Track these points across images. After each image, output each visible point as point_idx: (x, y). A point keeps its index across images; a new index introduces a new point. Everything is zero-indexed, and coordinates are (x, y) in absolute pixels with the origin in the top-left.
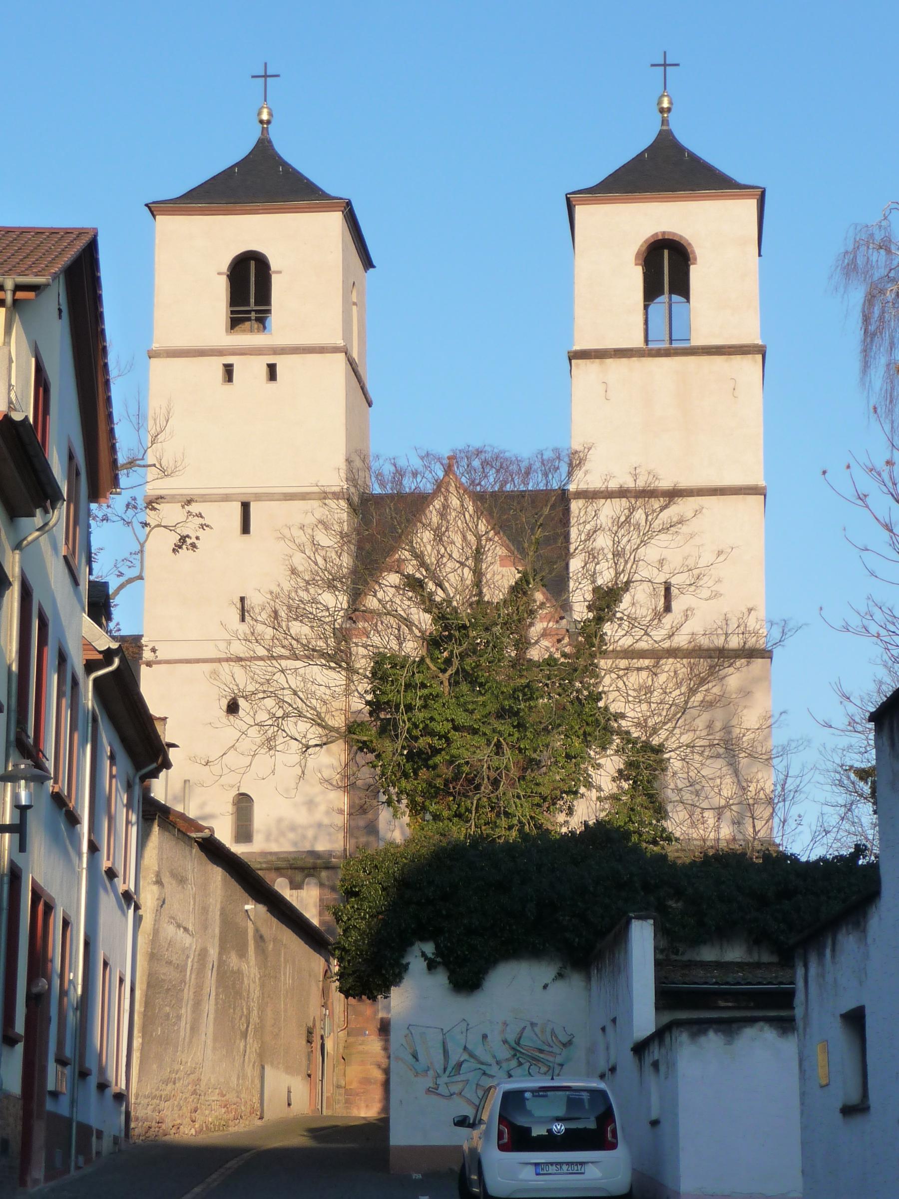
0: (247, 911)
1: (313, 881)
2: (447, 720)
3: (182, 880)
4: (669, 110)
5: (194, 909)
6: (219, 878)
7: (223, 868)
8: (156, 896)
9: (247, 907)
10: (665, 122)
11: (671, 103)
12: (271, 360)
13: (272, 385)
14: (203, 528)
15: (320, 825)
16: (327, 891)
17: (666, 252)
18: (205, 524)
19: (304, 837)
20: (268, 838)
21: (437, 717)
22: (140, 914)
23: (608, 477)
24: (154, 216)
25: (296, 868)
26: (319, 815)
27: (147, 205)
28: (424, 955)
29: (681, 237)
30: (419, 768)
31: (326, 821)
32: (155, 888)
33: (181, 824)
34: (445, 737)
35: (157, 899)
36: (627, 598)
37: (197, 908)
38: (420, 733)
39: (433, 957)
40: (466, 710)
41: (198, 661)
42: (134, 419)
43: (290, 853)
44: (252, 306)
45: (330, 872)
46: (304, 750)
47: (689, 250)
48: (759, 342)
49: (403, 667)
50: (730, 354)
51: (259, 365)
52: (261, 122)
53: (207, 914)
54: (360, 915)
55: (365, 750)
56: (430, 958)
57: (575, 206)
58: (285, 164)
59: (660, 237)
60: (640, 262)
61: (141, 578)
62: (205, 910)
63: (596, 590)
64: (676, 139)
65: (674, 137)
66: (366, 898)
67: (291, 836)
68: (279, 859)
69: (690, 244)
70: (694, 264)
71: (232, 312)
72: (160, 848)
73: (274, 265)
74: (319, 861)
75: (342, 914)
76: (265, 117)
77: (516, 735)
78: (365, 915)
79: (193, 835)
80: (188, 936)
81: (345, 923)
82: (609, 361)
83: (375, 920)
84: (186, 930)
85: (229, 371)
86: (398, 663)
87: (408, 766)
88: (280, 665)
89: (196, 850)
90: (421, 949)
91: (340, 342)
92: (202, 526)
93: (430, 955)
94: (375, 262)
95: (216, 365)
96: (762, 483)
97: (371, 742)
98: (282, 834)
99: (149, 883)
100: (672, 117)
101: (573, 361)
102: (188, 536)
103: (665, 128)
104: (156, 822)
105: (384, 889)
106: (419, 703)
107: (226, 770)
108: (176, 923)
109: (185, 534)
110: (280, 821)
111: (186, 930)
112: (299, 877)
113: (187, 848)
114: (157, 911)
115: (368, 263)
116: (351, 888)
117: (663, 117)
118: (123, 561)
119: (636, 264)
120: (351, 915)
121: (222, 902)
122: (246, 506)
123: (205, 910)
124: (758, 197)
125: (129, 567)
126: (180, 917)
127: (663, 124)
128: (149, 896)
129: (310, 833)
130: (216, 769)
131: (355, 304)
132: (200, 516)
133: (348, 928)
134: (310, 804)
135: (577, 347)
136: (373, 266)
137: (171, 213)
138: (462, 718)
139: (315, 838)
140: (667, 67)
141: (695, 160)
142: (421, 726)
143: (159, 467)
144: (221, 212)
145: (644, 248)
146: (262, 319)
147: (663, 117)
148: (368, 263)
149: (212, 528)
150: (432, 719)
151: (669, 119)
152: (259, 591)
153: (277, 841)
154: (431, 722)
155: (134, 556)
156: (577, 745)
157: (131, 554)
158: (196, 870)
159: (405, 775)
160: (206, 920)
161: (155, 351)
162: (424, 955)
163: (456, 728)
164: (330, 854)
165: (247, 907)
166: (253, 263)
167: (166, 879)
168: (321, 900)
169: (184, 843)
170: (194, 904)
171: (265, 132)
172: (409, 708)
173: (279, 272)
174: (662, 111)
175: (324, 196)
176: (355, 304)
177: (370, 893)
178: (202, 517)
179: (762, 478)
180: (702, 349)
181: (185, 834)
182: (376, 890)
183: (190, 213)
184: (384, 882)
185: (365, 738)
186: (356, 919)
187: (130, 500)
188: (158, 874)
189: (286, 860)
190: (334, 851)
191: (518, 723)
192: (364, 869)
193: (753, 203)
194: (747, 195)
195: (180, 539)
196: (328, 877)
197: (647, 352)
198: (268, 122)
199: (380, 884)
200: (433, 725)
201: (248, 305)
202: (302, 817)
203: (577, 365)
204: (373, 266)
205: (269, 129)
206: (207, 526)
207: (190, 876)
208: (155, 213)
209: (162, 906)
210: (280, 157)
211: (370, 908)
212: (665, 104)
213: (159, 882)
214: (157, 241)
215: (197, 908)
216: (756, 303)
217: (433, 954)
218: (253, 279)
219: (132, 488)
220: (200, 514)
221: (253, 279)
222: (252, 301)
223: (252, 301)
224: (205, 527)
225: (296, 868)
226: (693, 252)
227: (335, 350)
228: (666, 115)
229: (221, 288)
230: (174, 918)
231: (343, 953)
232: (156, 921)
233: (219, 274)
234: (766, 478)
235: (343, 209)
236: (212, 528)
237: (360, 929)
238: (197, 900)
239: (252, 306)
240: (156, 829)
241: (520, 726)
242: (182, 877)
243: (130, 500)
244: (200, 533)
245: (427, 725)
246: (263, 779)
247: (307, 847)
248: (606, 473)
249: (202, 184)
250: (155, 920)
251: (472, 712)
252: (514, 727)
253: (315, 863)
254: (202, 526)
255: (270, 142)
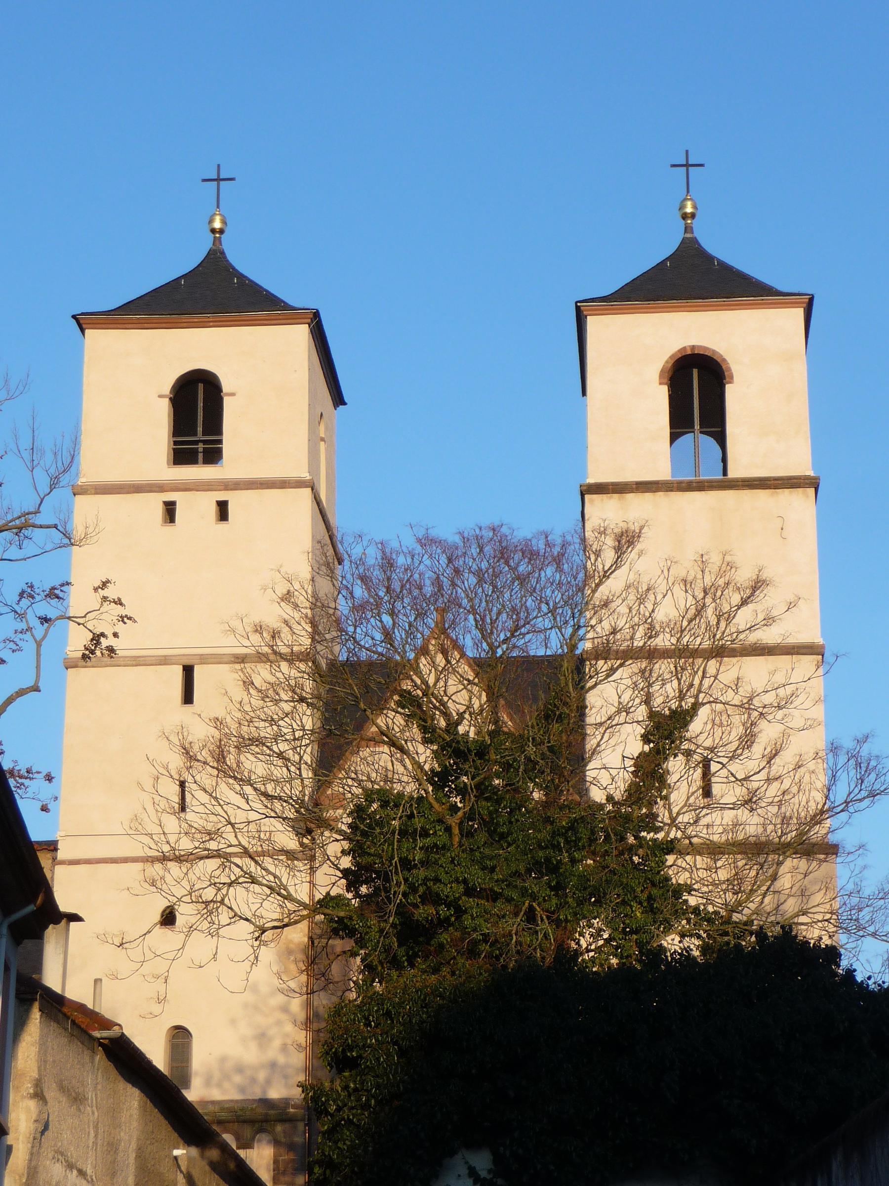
0: (176, 1158)
1: (264, 1137)
2: (457, 881)
3: (77, 1099)
4: (693, 216)
5: (95, 1143)
6: (136, 1104)
7: (142, 1090)
8: (34, 1117)
9: (176, 1152)
10: (689, 230)
11: (695, 207)
12: (222, 496)
13: (223, 525)
14: (123, 621)
15: (273, 1065)
16: (282, 1150)
17: (695, 372)
18: (126, 616)
19: (253, 1080)
20: (208, 1082)
21: (443, 877)
22: (9, 1143)
23: (669, 562)
24: (83, 331)
25: (244, 1122)
26: (273, 1052)
27: (74, 317)
28: (472, 1173)
29: (714, 351)
30: (416, 955)
31: (281, 1059)
32: (32, 1104)
33: (80, 1019)
34: (453, 904)
35: (36, 1121)
36: (695, 727)
37: (100, 1142)
38: (419, 900)
39: (489, 1177)
40: (484, 868)
41: (125, 860)
42: (26, 455)
43: (237, 1101)
44: (200, 436)
45: (287, 1125)
46: (257, 934)
47: (724, 367)
48: (811, 473)
49: (397, 806)
50: (776, 487)
51: (208, 502)
52: (213, 231)
53: (116, 1151)
54: (359, 1099)
55: (341, 933)
56: (485, 1179)
57: (586, 317)
58: (241, 276)
59: (689, 352)
60: (666, 380)
61: (35, 688)
62: (112, 1147)
63: (652, 715)
64: (701, 247)
65: (699, 244)
66: (371, 1069)
67: (238, 1079)
68: (222, 1109)
69: (724, 360)
70: (730, 383)
71: (175, 443)
72: (43, 1044)
73: (226, 387)
74: (272, 1112)
75: (327, 1101)
76: (217, 225)
77: (554, 901)
78: (368, 1100)
79: (97, 1034)
80: (85, 1182)
81: (332, 1115)
82: (630, 496)
83: (387, 1108)
84: (82, 1173)
85: (170, 510)
86: (388, 800)
87: (401, 952)
88: (226, 812)
89: (100, 1057)
90: (467, 1163)
91: (306, 475)
92: (123, 619)
93: (483, 1174)
94: (346, 399)
95: (155, 503)
96: (819, 640)
97: (351, 918)
98: (226, 1077)
99: (23, 1097)
100: (696, 224)
101: (586, 496)
102: (103, 635)
103: (688, 235)
104: (36, 1006)
105: (402, 1053)
106: (418, 856)
107: (148, 955)
108: (67, 1161)
109: (98, 631)
110: (223, 1060)
111: (82, 1173)
112: (247, 1131)
113: (87, 1053)
114: (34, 1139)
115: (338, 399)
116: (344, 1051)
117: (686, 224)
118: (4, 641)
119: (660, 384)
120: (342, 1101)
121: (138, 1139)
122: (188, 671)
123: (112, 1147)
124: (805, 305)
125: (13, 651)
126: (73, 1153)
127: (686, 232)
128: (23, 1117)
129: (262, 1076)
130: (135, 953)
131: (322, 439)
132: (119, 602)
133: (338, 1124)
134: (262, 1038)
135: (591, 480)
136: (344, 403)
137: (103, 326)
138: (478, 878)
139: (268, 1082)
140: (690, 168)
141: (726, 270)
142: (421, 890)
143: (62, 530)
144: (164, 325)
145: (670, 365)
146: (213, 456)
147: (686, 224)
148: (338, 399)
149: (135, 621)
150: (437, 880)
151: (693, 226)
152: (200, 715)
153: (219, 1085)
154: (434, 884)
155: (20, 636)
156: (638, 915)
157: (16, 632)
158: (99, 1087)
159: (395, 963)
160: (114, 1162)
161: (81, 486)
162: (472, 1173)
163: (470, 892)
164: (286, 1102)
165: (176, 1152)
166: (201, 386)
167: (51, 1093)
168: (276, 1162)
169: (83, 1043)
170: (96, 1136)
171: (217, 242)
172: (406, 864)
173: (232, 394)
174: (685, 216)
175: (286, 307)
176: (322, 439)
177: (378, 1059)
178: (121, 604)
179: (819, 634)
180: (738, 486)
181: (85, 1032)
182: (389, 1055)
183: (127, 326)
184: (403, 1038)
185: (342, 914)
186: (352, 1108)
187: (25, 587)
188: (38, 1084)
189: (230, 1110)
190: (293, 1100)
191: (557, 883)
192: (367, 1019)
193: (800, 312)
194: (792, 303)
195: (92, 640)
196: (284, 1132)
197: (675, 485)
198: (221, 231)
199: (395, 1043)
200: (436, 888)
201: (195, 434)
202: (251, 1055)
203: (592, 501)
204: (344, 403)
205: (222, 239)
206: (130, 618)
207: (90, 1095)
208: (84, 326)
209: (42, 1133)
210: (234, 268)
211: (378, 1087)
212: (689, 209)
213: (39, 1095)
214: (86, 359)
215: (100, 1142)
216: (806, 428)
217: (489, 1171)
218: (201, 404)
219: (25, 559)
220: (119, 599)
221: (201, 404)
222: (200, 429)
223: (200, 429)
224: (125, 619)
225: (244, 1122)
226: (729, 369)
227: (299, 484)
228: (689, 222)
229: (162, 412)
230: (62, 1154)
231: (328, 1172)
232: (34, 1155)
233: (160, 396)
234: (823, 635)
235: (309, 321)
236: (135, 621)
237: (358, 1126)
238: (100, 1131)
239: (200, 436)
240: (36, 1015)
241: (558, 888)
242: (78, 1094)
243: (25, 587)
244: (120, 628)
245: (428, 888)
246: (201, 967)
247: (256, 1093)
248: (666, 557)
249: (142, 296)
250: (32, 1154)
251: (492, 870)
252: (552, 888)
253: (266, 1115)
254: (123, 619)
255: (223, 253)
